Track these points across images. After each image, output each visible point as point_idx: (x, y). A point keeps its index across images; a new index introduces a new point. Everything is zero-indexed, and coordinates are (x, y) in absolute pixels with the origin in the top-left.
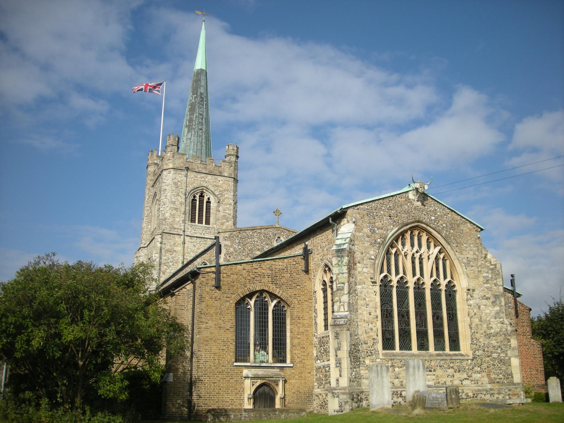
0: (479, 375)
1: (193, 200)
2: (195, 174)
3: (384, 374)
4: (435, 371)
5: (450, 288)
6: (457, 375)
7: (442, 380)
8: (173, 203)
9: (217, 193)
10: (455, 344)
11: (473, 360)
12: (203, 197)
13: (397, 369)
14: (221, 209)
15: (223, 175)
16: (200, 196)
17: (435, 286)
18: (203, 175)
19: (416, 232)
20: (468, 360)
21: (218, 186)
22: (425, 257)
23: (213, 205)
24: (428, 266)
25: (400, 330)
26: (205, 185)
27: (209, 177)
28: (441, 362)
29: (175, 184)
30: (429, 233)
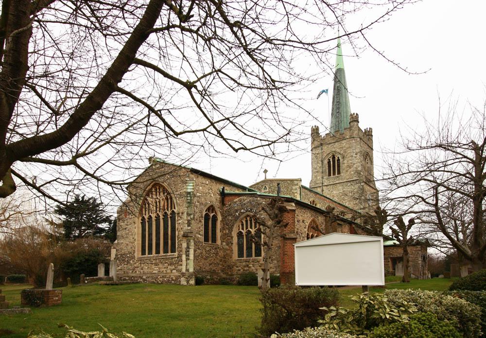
1: (328, 162)
2: (327, 146)
6: (169, 267)
8: (316, 169)
9: (342, 152)
11: (178, 258)
14: (345, 162)
15: (346, 138)
16: (333, 158)
18: (332, 144)
20: (175, 258)
26: (334, 150)
27: (337, 144)
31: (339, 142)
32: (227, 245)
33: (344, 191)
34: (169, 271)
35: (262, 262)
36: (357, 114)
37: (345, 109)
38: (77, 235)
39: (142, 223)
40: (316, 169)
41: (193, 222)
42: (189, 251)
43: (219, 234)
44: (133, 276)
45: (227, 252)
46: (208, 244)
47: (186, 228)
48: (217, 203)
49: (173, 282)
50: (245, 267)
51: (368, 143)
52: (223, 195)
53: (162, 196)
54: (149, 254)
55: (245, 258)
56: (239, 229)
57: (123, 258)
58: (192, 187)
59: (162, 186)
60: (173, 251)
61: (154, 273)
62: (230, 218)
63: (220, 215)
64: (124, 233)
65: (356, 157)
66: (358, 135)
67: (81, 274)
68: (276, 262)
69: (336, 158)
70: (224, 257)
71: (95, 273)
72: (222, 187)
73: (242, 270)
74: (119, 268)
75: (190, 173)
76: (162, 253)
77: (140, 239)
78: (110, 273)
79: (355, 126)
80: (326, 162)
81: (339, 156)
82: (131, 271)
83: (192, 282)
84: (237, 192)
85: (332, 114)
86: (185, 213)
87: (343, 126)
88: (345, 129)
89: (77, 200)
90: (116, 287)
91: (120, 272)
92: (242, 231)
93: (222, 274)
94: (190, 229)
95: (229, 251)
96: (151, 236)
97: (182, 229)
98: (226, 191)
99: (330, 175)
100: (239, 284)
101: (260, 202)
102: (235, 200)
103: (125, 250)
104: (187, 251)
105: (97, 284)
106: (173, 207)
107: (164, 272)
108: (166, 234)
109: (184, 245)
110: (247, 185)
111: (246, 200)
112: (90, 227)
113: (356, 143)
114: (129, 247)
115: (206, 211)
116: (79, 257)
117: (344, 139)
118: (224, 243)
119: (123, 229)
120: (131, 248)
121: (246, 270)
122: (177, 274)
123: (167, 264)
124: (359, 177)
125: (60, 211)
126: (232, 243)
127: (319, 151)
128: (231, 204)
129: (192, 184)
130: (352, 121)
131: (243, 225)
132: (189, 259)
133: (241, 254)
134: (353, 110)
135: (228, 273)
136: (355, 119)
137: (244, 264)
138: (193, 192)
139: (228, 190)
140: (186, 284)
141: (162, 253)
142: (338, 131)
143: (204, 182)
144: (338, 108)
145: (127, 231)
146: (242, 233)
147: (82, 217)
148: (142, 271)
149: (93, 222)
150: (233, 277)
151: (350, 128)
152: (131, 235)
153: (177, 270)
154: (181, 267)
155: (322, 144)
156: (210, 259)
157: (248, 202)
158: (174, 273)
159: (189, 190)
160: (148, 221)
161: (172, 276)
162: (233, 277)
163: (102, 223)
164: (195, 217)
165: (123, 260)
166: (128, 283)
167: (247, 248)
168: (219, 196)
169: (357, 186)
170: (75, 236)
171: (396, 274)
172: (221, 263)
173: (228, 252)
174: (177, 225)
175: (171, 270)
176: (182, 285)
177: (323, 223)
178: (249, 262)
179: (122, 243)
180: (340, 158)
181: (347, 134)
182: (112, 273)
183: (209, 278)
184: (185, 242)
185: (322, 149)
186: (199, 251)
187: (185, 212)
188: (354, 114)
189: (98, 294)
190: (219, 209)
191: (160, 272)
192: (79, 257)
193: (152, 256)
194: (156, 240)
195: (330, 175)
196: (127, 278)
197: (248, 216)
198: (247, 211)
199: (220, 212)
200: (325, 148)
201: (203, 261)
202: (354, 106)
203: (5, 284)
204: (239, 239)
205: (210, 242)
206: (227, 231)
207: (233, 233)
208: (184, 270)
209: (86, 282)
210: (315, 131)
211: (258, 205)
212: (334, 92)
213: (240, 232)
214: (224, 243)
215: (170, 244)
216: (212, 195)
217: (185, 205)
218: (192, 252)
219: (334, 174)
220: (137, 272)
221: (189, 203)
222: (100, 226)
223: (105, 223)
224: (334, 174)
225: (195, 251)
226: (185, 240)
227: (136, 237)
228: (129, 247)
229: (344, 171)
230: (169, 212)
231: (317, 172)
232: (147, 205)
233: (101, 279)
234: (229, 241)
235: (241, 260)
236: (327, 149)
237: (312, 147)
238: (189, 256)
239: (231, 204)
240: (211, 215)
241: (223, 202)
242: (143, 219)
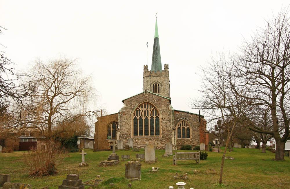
0: (164, 142)
3: (121, 142)
5: (157, 119)
9: (161, 82)
10: (158, 134)
11: (162, 138)
14: (162, 87)
17: (152, 118)
18: (156, 77)
19: (146, 104)
21: (161, 80)
22: (149, 110)
23: (160, 86)
24: (149, 113)
25: (145, 131)
26: (157, 80)
27: (158, 77)
29: (147, 82)
30: (150, 104)
49: (159, 149)
50: (182, 142)
68: (197, 141)
69: (158, 85)
80: (152, 85)
81: (159, 84)
102: (177, 113)
103: (124, 132)
121: (183, 144)
127: (148, 79)
131: (180, 124)
148: (136, 143)
155: (150, 76)
175: (158, 144)
197: (184, 121)
200: (152, 78)
202: (164, 61)
210: (146, 67)
213: (179, 127)
229: (162, 92)
236: (153, 79)
237: (144, 75)
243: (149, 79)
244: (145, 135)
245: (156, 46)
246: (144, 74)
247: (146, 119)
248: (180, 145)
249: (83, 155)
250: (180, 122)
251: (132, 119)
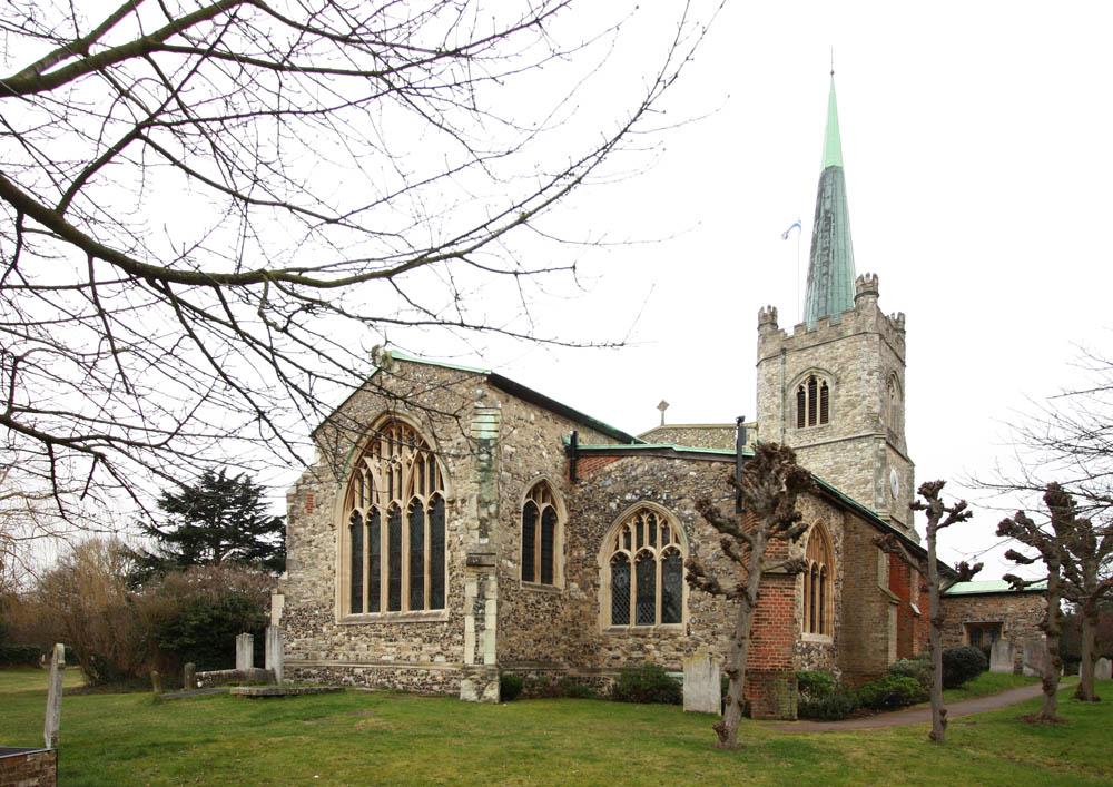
1: (799, 394)
2: (798, 353)
4: (396, 640)
6: (426, 647)
7: (404, 654)
8: (767, 409)
9: (834, 370)
11: (450, 622)
12: (816, 383)
13: (353, 638)
14: (842, 392)
16: (810, 384)
20: (443, 623)
23: (831, 390)
26: (814, 364)
27: (821, 348)
28: (406, 628)
29: (769, 380)
31: (828, 346)
32: (583, 589)
33: (836, 463)
34: (425, 658)
35: (683, 638)
36: (875, 276)
37: (842, 269)
38: (211, 558)
39: (352, 528)
40: (767, 409)
41: (494, 524)
42: (483, 607)
43: (560, 559)
44: (328, 668)
45: (582, 607)
46: (532, 586)
47: (475, 541)
48: (556, 476)
49: (436, 687)
50: (633, 649)
51: (896, 348)
52: (573, 453)
53: (408, 455)
54: (370, 611)
55: (632, 626)
56: (617, 548)
57: (301, 619)
58: (493, 427)
59: (407, 426)
60: (437, 603)
61: (384, 663)
62: (592, 517)
63: (564, 511)
64: (304, 552)
65: (868, 381)
66: (877, 326)
67: (186, 662)
69: (819, 384)
70: (574, 622)
71: (229, 658)
72: (572, 432)
73: (624, 659)
74: (293, 645)
75: (485, 386)
76: (405, 609)
77: (349, 572)
78: (268, 661)
79: (870, 305)
80: (793, 393)
81: (828, 379)
82: (323, 654)
83: (493, 692)
84: (616, 446)
85: (810, 279)
86: (474, 499)
87: (836, 306)
88: (845, 313)
89: (208, 479)
90: (276, 704)
91: (296, 656)
92: (626, 552)
93: (566, 666)
94: (486, 545)
95: (588, 606)
96: (376, 562)
97: (461, 544)
98: (581, 445)
99: (801, 423)
100: (619, 696)
101: (683, 471)
104: (479, 607)
105: (225, 694)
106: (437, 485)
107: (413, 659)
108: (416, 557)
109: (472, 590)
110: (634, 433)
111: (641, 465)
112: (237, 539)
113: (870, 346)
114: (319, 592)
115: (527, 497)
116: (196, 613)
117: (841, 336)
118: (575, 585)
119: (302, 544)
120: (325, 593)
121: (637, 659)
122: (448, 667)
123: (419, 639)
124: (875, 428)
125: (170, 504)
126: (599, 586)
127: (775, 368)
128: (594, 479)
129: (492, 419)
130: (862, 295)
131: (627, 535)
132: (483, 629)
133: (620, 615)
134: (862, 265)
135: (583, 664)
136: (870, 288)
137: (631, 641)
138: (496, 439)
139: (586, 441)
140: (476, 698)
141: (405, 609)
142: (826, 318)
143: (524, 415)
144: (827, 264)
145: (314, 550)
146: (627, 557)
147: (220, 519)
148: (352, 654)
149: (246, 529)
150: (597, 675)
151: (857, 312)
152: (322, 566)
153: (447, 657)
154: (459, 648)
155: (784, 351)
156: (537, 627)
157: (645, 473)
158: (438, 664)
159: (485, 435)
160: (369, 524)
161: (432, 673)
162: (597, 675)
163: (266, 532)
164: (501, 511)
165: (303, 625)
166: (322, 690)
167: (640, 600)
168: (562, 457)
169: (870, 451)
170: (206, 562)
171: (992, 667)
172: (563, 637)
173: (586, 608)
174: (447, 533)
176: (465, 701)
177: (838, 534)
178: (643, 637)
179: (301, 580)
180: (829, 385)
181: (850, 326)
182: (273, 660)
183: (535, 677)
184: (472, 581)
185: (784, 363)
186: (507, 606)
187: (471, 496)
188: (868, 275)
189: (209, 741)
190: (561, 493)
191: (399, 658)
192: (196, 613)
193: (379, 614)
194: (391, 574)
195: (801, 423)
196: (314, 672)
197: (645, 510)
198: (640, 499)
199: (565, 501)
200: (792, 358)
201: (519, 632)
202: (864, 258)
203: (44, 667)
204: (615, 573)
205: (538, 582)
206: (584, 553)
207: (599, 557)
208: (469, 660)
209: (199, 684)
210: (768, 320)
211: (676, 479)
212: (817, 225)
213: (621, 554)
214: (575, 585)
215: (429, 586)
216: (544, 454)
217: (474, 475)
218: (491, 608)
219: (813, 422)
220: (341, 657)
221: (483, 470)
222: (260, 538)
223: (273, 531)
224: (813, 422)
225: (499, 605)
226: (471, 574)
227: (337, 566)
228: (319, 592)
230: (425, 500)
231: (771, 417)
232: (366, 479)
233: (240, 678)
234: (588, 578)
235: (622, 630)
236: (796, 364)
237: (759, 356)
238: (483, 620)
239: (594, 479)
240: (542, 507)
241: (572, 476)
242: (356, 517)
243: (780, 367)
244: (663, 622)
245: (828, 205)
246: (759, 348)
247: (395, 513)
248: (616, 664)
249: (53, 694)
250: (620, 518)
251: (338, 525)
